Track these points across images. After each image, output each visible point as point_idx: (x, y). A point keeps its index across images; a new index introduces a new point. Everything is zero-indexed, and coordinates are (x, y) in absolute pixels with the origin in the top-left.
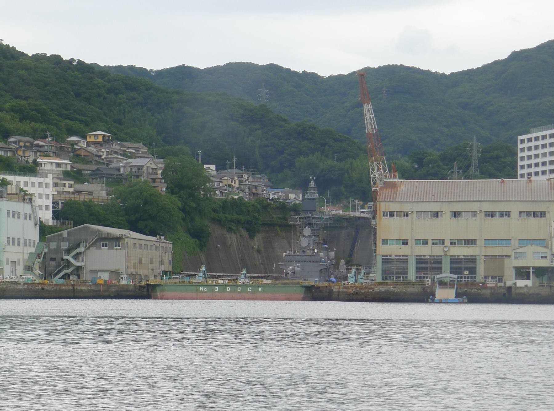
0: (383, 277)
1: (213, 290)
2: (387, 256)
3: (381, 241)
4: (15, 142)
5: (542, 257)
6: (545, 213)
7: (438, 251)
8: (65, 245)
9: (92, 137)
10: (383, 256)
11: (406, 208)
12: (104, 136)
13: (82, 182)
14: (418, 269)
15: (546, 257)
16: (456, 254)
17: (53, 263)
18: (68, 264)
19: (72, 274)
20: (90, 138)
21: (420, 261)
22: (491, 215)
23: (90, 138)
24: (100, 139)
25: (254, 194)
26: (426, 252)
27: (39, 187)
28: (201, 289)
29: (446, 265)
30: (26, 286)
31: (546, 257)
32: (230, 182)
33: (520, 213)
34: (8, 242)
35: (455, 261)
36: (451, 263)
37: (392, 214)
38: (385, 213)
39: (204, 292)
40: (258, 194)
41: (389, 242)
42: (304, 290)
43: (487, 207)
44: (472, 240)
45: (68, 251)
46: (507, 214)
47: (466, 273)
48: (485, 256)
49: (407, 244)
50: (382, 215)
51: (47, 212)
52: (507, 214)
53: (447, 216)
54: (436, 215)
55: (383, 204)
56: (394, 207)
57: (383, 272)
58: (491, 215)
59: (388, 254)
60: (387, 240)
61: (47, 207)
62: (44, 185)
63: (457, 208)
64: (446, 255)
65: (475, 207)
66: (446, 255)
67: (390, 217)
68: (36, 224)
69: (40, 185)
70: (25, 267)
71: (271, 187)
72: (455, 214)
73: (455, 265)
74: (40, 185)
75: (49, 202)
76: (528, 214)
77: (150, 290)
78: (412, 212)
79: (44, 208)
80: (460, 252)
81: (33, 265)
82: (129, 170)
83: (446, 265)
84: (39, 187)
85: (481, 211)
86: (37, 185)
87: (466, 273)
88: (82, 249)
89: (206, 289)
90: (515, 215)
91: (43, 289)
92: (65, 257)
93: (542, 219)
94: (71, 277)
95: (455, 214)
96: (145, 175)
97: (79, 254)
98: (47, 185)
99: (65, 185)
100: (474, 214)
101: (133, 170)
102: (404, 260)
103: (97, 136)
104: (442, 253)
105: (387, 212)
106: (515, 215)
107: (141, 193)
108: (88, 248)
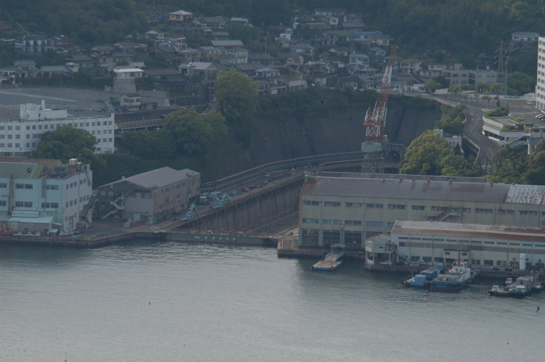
0: (302, 243)
4: (97, 52)
5: (380, 247)
6: (404, 206)
7: (337, 228)
8: (111, 194)
9: (175, 17)
11: (318, 199)
12: (185, 16)
14: (325, 238)
15: (382, 247)
16: (348, 230)
17: (103, 206)
18: (114, 208)
19: (116, 214)
20: (173, 17)
21: (326, 233)
22: (370, 206)
23: (173, 17)
24: (182, 19)
26: (329, 227)
27: (104, 125)
29: (342, 237)
30: (75, 242)
31: (382, 247)
32: (293, 63)
33: (389, 205)
34: (67, 206)
35: (348, 234)
36: (345, 235)
37: (309, 202)
38: (305, 202)
40: (319, 72)
43: (368, 201)
44: (359, 222)
45: (114, 198)
46: (381, 206)
47: (355, 242)
48: (367, 232)
51: (110, 143)
52: (381, 206)
53: (343, 206)
54: (338, 204)
55: (303, 196)
56: (310, 198)
58: (370, 206)
61: (110, 140)
62: (108, 123)
63: (350, 200)
64: (342, 230)
65: (361, 200)
66: (342, 230)
68: (89, 184)
69: (105, 123)
70: (80, 216)
71: (364, 29)
72: (349, 205)
74: (105, 123)
75: (112, 136)
76: (394, 206)
78: (321, 202)
79: (108, 141)
80: (351, 228)
81: (86, 215)
82: (193, 73)
83: (342, 237)
84: (104, 125)
85: (364, 204)
86: (102, 124)
87: (355, 242)
88: (123, 198)
90: (386, 207)
91: (86, 244)
92: (112, 203)
93: (403, 210)
94: (115, 217)
95: (349, 205)
96: (206, 78)
97: (121, 200)
98: (110, 123)
99: (132, 101)
100: (360, 205)
101: (197, 74)
102: (316, 232)
103: (178, 16)
104: (339, 229)
106: (386, 207)
107: (186, 121)
108: (128, 197)
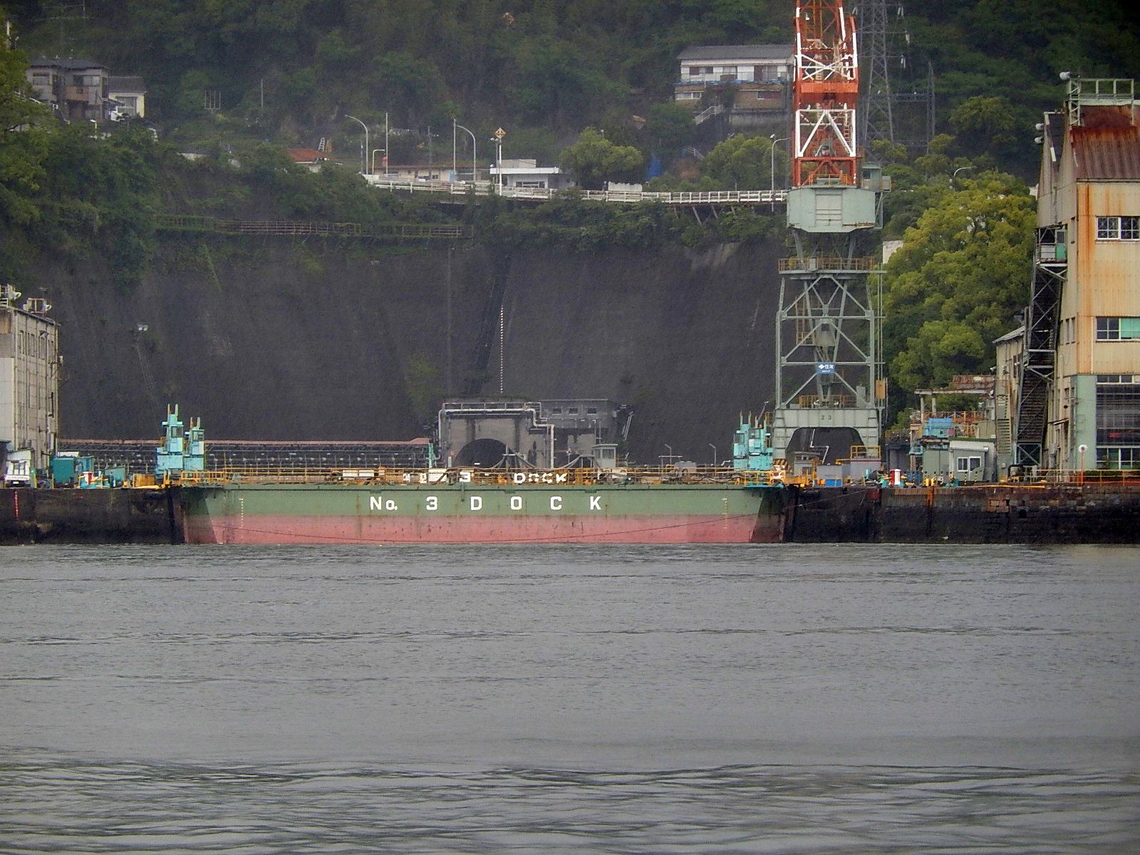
0: (1101, 453)
1: (420, 506)
2: (1114, 378)
3: (1093, 324)
10: (1101, 378)
13: (428, 222)
25: (73, 104)
28: (375, 503)
38: (1106, 224)
39: (383, 515)
40: (85, 105)
41: (1123, 329)
42: (755, 504)
49: (1101, 321)
50: (1096, 230)
57: (1102, 437)
59: (1121, 369)
60: (1114, 322)
67: (1126, 235)
73: (804, 322)
77: (177, 506)
89: (391, 505)
105: (1114, 219)
